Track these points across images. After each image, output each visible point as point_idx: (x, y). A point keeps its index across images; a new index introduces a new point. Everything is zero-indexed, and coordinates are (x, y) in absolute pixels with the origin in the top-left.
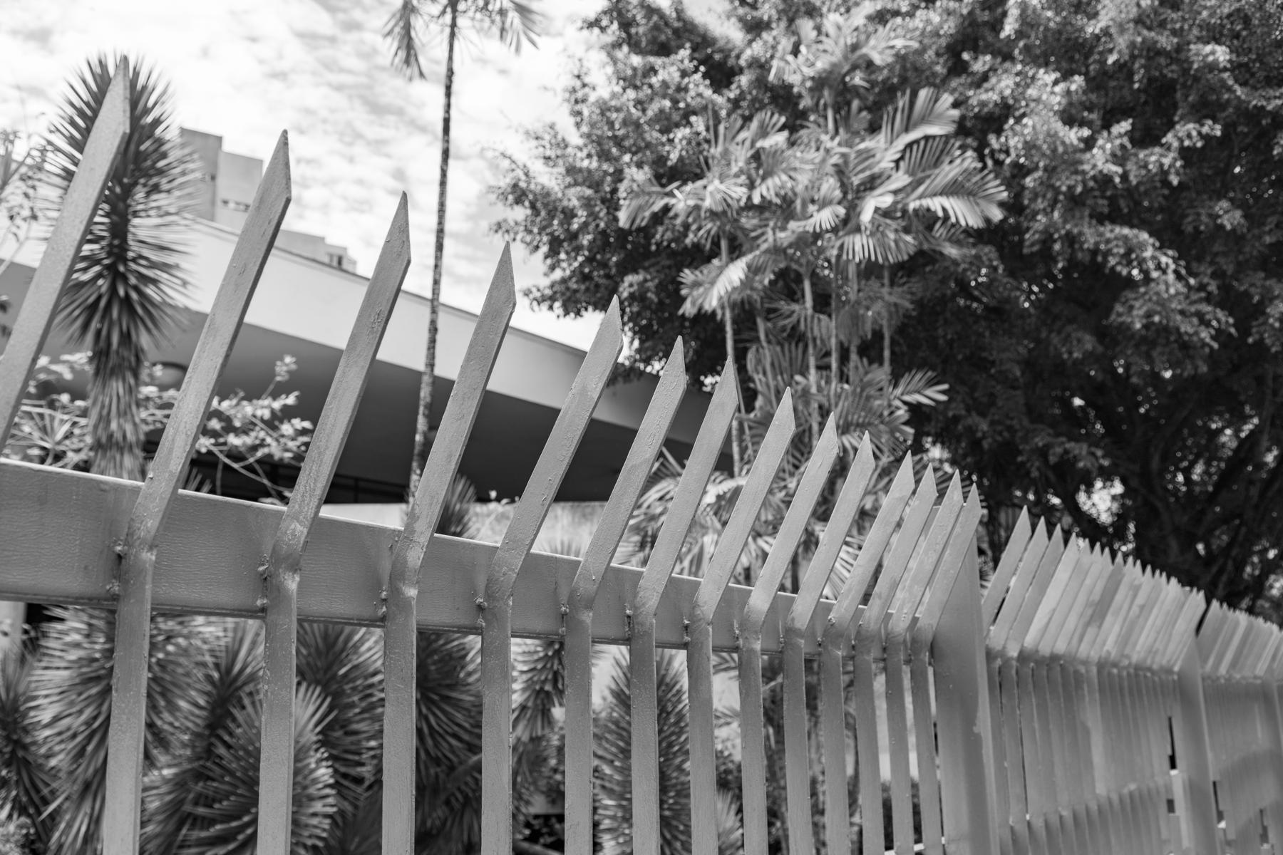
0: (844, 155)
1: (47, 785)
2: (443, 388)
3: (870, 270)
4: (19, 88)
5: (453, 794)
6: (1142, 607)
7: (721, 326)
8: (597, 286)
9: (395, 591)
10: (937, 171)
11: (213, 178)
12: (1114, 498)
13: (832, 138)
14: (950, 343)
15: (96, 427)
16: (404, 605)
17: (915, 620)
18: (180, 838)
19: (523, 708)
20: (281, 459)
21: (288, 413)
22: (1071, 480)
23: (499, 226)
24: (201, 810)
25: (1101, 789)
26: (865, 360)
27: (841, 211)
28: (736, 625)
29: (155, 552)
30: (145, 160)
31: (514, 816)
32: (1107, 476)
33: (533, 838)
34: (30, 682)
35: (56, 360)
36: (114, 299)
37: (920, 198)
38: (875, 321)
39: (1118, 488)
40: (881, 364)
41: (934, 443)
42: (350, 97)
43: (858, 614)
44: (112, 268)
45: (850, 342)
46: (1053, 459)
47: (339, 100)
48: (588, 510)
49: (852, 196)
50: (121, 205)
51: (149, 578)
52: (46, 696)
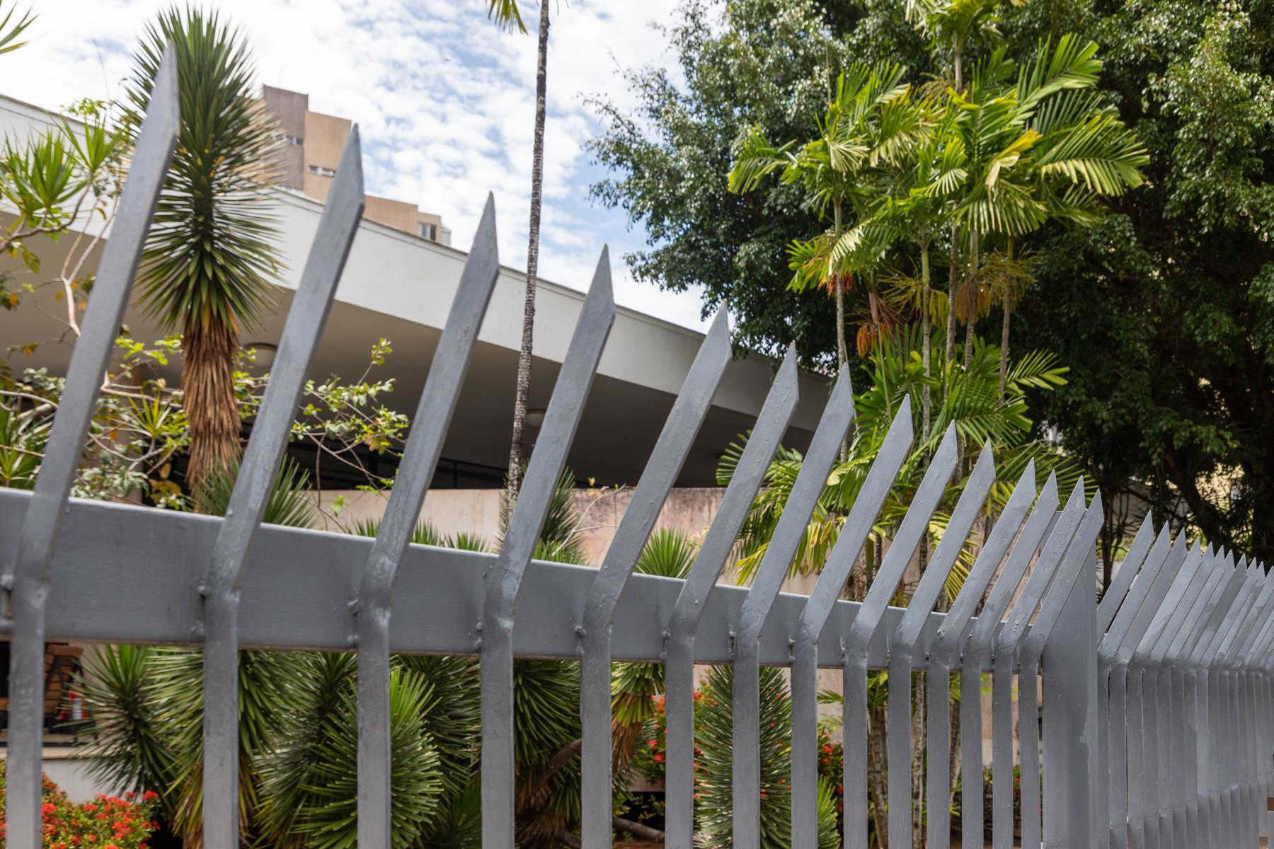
0: (971, 112)
1: (171, 762)
2: (546, 373)
3: (993, 242)
4: (95, 43)
5: (556, 775)
6: (1261, 609)
7: (833, 302)
8: (704, 255)
9: (491, 623)
10: (1074, 129)
11: (300, 142)
12: (1234, 482)
13: (960, 93)
14: (1074, 321)
15: (192, 415)
16: (500, 636)
17: (1027, 629)
18: (297, 814)
19: (624, 695)
20: (376, 451)
21: (383, 400)
22: (1192, 463)
23: (600, 187)
24: (315, 789)
25: (1202, 791)
26: (982, 339)
27: (963, 174)
28: (842, 642)
29: (238, 593)
30: (227, 128)
31: (614, 795)
32: (1230, 462)
33: (632, 816)
34: (146, 666)
35: (150, 346)
36: (202, 278)
37: (1052, 161)
38: (995, 297)
39: (1239, 472)
40: (999, 345)
41: (1050, 426)
42: (440, 48)
43: (970, 624)
44: (198, 247)
45: (967, 319)
46: (1177, 444)
47: (429, 51)
48: (689, 496)
49: (977, 159)
50: (203, 178)
51: (234, 621)
52: (161, 681)
